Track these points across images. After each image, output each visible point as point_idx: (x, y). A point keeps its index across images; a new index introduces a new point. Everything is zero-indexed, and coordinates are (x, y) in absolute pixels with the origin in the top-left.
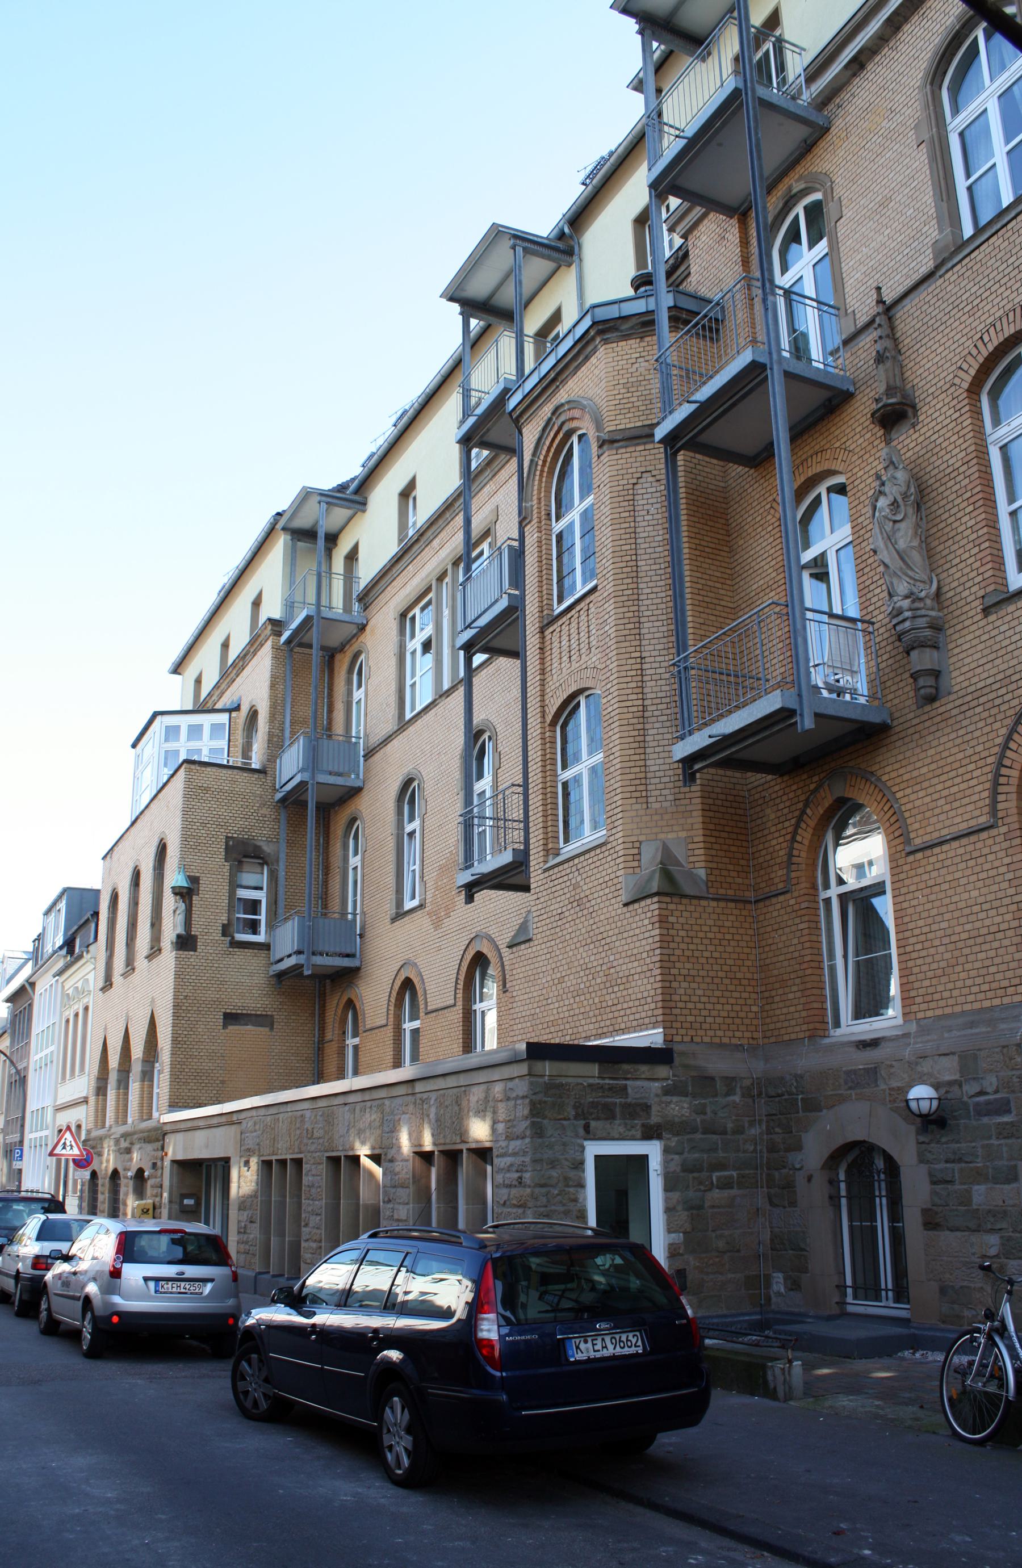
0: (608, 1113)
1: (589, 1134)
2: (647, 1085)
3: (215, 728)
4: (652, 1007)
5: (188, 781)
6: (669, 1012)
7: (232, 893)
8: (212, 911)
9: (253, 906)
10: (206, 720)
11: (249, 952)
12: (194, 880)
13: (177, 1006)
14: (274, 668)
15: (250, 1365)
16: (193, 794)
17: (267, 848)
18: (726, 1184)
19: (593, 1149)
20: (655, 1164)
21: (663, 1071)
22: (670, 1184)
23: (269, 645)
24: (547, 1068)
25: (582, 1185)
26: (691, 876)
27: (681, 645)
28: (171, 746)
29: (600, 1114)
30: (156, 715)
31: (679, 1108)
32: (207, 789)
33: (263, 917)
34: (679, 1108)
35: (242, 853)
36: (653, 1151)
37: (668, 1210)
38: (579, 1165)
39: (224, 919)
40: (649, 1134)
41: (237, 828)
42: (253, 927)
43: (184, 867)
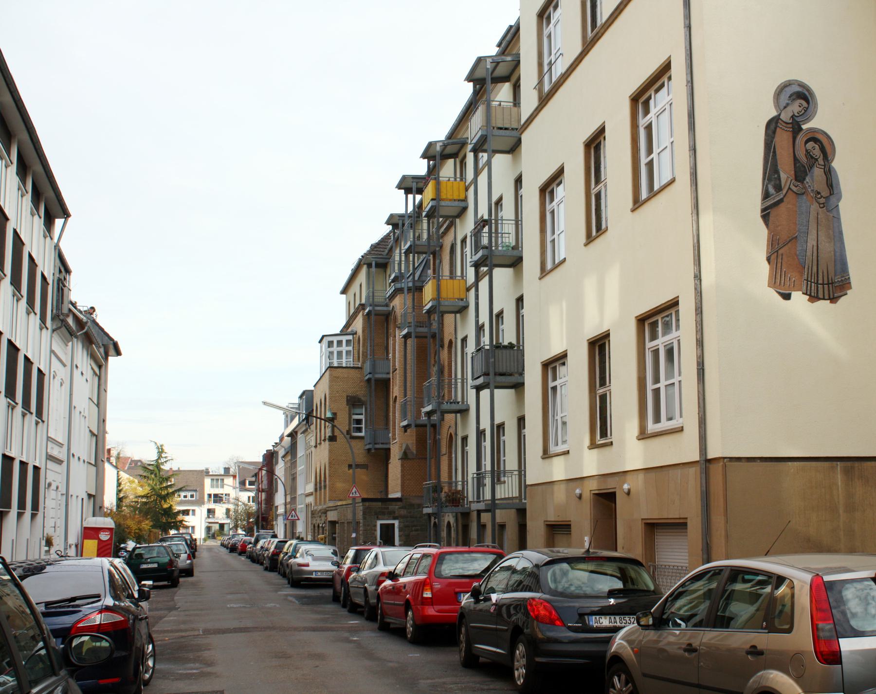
0: (383, 513)
1: (378, 519)
2: (394, 507)
3: (348, 342)
4: (399, 488)
5: (330, 375)
6: (403, 490)
7: (350, 417)
8: (343, 422)
9: (359, 422)
10: (344, 339)
11: (358, 440)
12: (335, 414)
13: (330, 463)
14: (364, 324)
15: (619, 680)
16: (333, 380)
17: (363, 399)
18: (417, 530)
19: (379, 523)
20: (396, 525)
21: (399, 503)
22: (400, 530)
23: (361, 314)
24: (367, 504)
25: (376, 530)
26: (412, 453)
27: (405, 396)
28: (331, 349)
29: (379, 515)
30: (323, 337)
31: (403, 512)
32: (338, 378)
33: (363, 426)
34: (403, 512)
35: (354, 402)
36: (396, 523)
37: (400, 536)
38: (375, 526)
39: (347, 428)
40: (394, 519)
41: (351, 392)
42: (359, 430)
43: (330, 410)
